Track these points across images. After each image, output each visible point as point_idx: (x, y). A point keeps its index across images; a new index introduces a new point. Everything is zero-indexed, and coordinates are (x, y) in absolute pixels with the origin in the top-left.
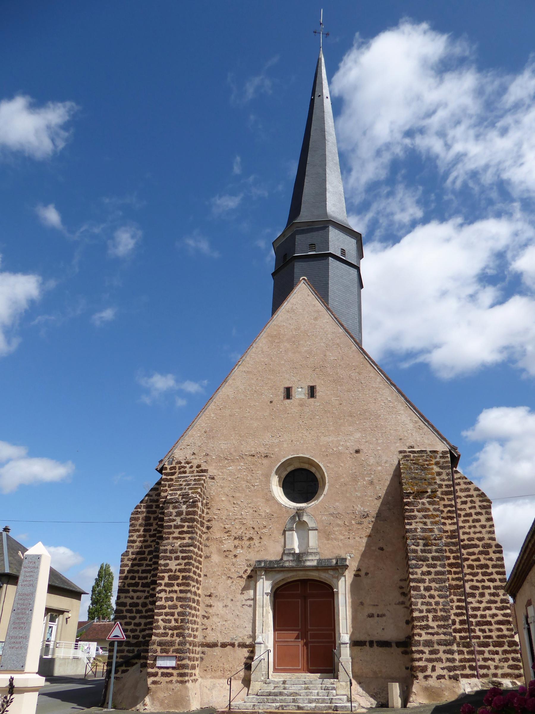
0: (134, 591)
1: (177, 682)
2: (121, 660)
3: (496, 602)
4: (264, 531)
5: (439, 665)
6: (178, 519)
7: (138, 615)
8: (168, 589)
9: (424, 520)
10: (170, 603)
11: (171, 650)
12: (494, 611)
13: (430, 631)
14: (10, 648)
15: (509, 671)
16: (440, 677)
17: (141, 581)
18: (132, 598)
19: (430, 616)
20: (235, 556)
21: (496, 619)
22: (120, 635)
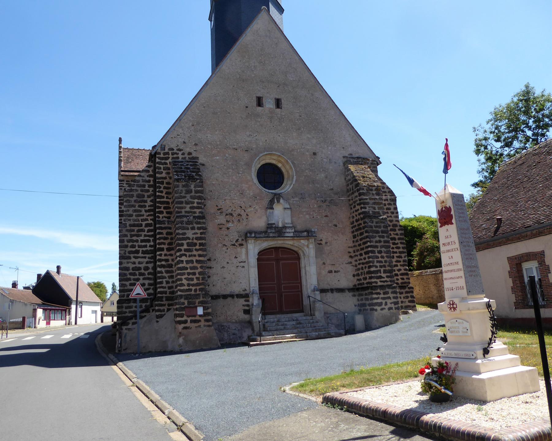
0: (136, 258)
1: (205, 326)
2: (131, 314)
3: (400, 262)
4: (250, 210)
5: (389, 301)
6: (188, 196)
7: (141, 277)
8: (188, 254)
9: (374, 206)
10: (191, 265)
11: (197, 302)
12: (399, 267)
13: (382, 280)
14: (470, 275)
15: (409, 304)
16: (390, 309)
17: (141, 249)
18: (134, 263)
19: (382, 270)
20: (228, 229)
21: (401, 272)
22: (142, 293)
